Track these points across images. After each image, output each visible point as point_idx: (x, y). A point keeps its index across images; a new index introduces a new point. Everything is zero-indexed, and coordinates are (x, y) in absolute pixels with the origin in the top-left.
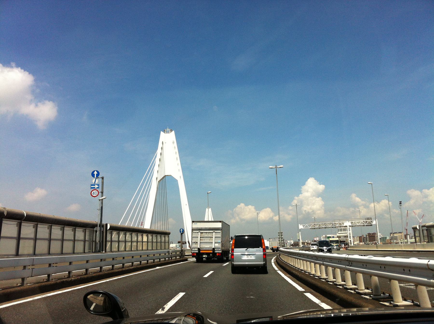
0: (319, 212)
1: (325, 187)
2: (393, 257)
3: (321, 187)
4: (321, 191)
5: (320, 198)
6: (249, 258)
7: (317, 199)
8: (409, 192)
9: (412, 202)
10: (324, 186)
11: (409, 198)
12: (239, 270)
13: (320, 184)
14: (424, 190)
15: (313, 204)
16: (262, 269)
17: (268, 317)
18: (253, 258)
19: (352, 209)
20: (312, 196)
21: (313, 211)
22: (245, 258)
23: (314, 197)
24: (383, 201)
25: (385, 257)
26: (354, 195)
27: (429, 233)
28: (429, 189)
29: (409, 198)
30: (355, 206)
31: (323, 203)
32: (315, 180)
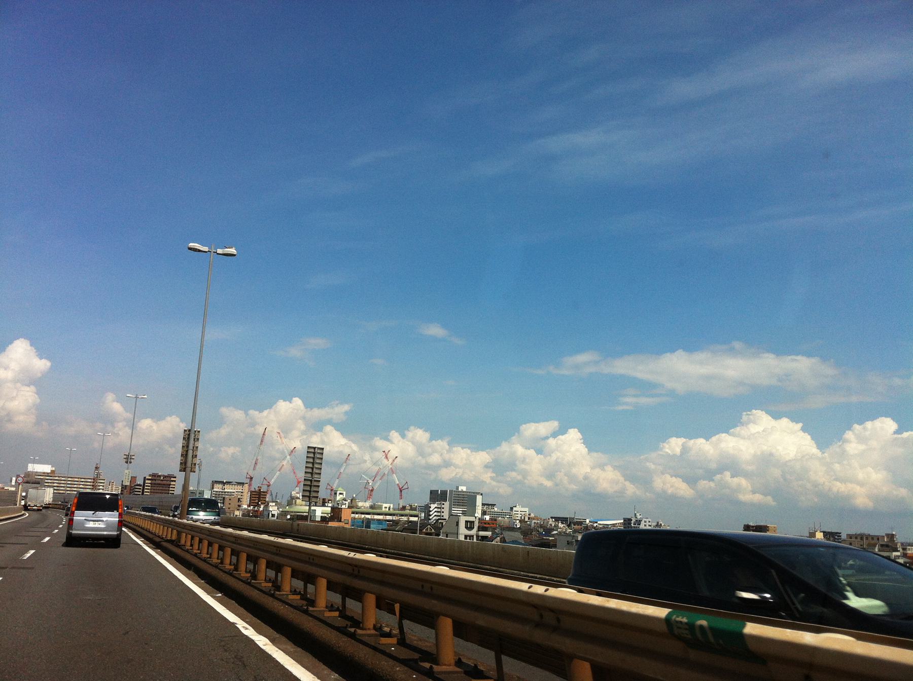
0: (22, 418)
1: (51, 368)
2: (580, 591)
3: (41, 365)
4: (39, 375)
5: (33, 388)
6: (97, 525)
7: (28, 389)
8: (224, 411)
9: (224, 431)
10: (48, 364)
11: (221, 422)
12: (74, 541)
13: (41, 358)
14: (251, 412)
15: (13, 399)
16: (113, 542)
17: (437, 651)
18: (102, 526)
19: (99, 425)
20: (15, 381)
21: (8, 415)
22: (91, 525)
23: (19, 385)
24: (169, 418)
25: (434, 565)
26: (110, 397)
27: (910, 617)
28: (261, 411)
29: (221, 422)
30: (109, 420)
31: (38, 401)
32: (29, 348)
